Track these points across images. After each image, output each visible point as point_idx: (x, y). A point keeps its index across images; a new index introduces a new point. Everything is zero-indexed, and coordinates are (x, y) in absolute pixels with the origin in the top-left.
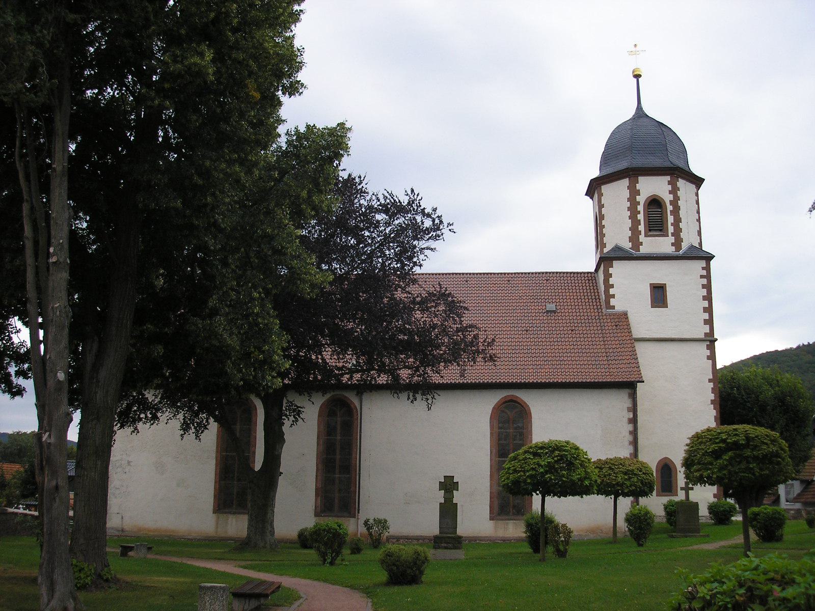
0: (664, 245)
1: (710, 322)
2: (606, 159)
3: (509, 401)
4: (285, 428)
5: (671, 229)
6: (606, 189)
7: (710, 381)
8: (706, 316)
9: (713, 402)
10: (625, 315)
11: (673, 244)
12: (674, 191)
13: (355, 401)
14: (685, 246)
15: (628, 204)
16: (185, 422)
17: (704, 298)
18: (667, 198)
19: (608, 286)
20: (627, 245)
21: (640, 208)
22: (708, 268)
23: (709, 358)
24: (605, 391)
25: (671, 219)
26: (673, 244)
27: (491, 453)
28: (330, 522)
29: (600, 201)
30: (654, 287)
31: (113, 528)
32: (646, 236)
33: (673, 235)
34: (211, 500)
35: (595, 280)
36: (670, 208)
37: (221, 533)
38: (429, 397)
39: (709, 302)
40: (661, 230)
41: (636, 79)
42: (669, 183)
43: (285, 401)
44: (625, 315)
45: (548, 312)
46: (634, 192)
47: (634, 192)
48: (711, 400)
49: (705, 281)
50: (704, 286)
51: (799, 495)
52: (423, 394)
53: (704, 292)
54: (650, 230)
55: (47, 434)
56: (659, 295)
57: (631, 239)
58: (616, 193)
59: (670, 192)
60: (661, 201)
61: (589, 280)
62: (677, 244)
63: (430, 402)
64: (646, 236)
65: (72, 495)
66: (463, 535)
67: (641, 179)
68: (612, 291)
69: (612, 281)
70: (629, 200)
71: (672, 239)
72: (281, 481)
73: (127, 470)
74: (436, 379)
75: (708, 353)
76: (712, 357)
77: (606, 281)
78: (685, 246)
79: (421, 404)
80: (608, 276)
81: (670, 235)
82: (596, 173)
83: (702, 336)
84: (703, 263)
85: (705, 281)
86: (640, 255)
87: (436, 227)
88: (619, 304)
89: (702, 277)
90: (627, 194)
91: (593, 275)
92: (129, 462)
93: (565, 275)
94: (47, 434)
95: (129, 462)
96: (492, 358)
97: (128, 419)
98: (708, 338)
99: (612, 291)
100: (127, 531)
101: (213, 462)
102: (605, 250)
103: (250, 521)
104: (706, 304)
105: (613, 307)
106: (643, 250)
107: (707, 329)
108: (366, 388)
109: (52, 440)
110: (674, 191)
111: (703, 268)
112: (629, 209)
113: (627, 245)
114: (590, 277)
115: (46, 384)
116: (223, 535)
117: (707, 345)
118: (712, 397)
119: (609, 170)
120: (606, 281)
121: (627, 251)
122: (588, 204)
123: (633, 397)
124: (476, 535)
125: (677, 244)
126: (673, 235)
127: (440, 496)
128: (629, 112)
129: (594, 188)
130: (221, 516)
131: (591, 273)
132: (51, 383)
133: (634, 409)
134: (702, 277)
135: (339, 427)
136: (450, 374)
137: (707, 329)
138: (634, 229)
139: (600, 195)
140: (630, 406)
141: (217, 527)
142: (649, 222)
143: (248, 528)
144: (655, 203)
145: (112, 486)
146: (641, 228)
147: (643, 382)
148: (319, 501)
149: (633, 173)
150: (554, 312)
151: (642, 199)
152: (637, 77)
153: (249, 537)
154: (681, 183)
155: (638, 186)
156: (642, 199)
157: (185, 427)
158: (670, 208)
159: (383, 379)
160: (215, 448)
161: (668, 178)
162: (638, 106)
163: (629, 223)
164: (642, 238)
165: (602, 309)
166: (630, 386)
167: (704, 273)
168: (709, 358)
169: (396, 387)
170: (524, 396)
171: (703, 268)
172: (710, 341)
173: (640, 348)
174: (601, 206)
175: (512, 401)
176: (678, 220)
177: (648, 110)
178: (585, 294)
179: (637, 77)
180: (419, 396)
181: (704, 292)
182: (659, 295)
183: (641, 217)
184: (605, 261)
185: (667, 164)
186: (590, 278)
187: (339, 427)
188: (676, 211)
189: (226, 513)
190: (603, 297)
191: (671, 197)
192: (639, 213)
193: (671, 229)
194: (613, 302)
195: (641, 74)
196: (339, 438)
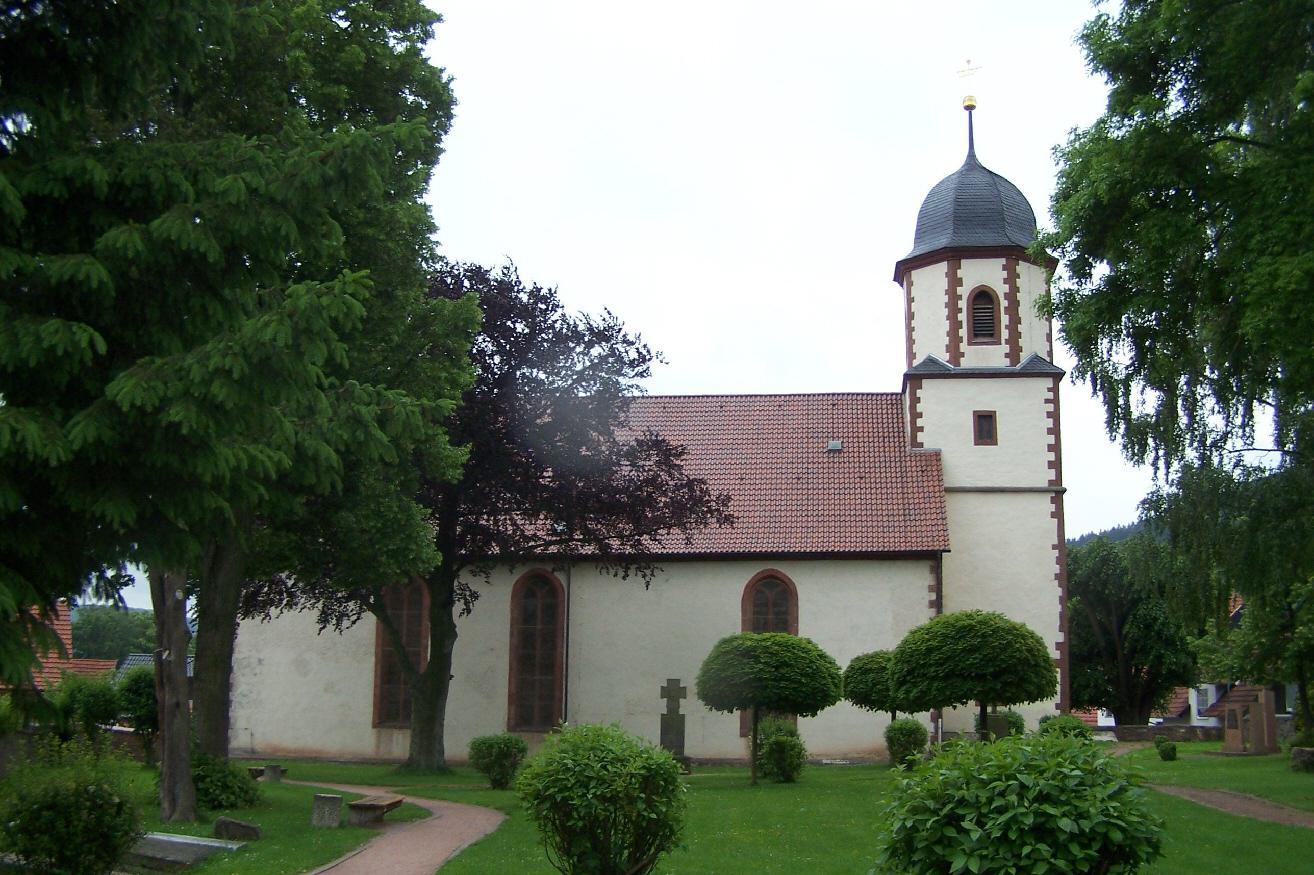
0: (995, 356)
1: (1056, 465)
2: (921, 233)
3: (765, 578)
4: (1158, 393)
5: (1005, 334)
6: (917, 275)
7: (1054, 547)
8: (1052, 456)
9: (1057, 577)
10: (937, 455)
11: (1007, 355)
12: (1012, 279)
13: (561, 577)
14: (1024, 357)
15: (946, 299)
16: (323, 612)
17: (1050, 431)
18: (1001, 289)
19: (916, 415)
20: (943, 357)
21: (963, 304)
22: (1055, 390)
23: (1053, 515)
24: (899, 563)
25: (1005, 319)
26: (1007, 355)
27: (511, 669)
28: (514, 736)
29: (909, 293)
30: (979, 416)
31: (238, 749)
32: (970, 344)
33: (1007, 342)
34: (370, 709)
35: (901, 404)
36: (1004, 303)
37: (384, 754)
38: (648, 572)
39: (1056, 437)
40: (991, 335)
41: (967, 112)
42: (1005, 268)
43: (456, 583)
44: (937, 455)
45: (830, 451)
46: (955, 282)
47: (955, 282)
48: (1056, 575)
49: (1051, 407)
50: (1049, 415)
51: (1212, 706)
52: (639, 569)
53: (1050, 423)
54: (976, 336)
55: (167, 652)
56: (985, 427)
57: (948, 349)
58: (932, 280)
59: (1006, 281)
60: (992, 293)
61: (892, 404)
62: (1014, 353)
63: (647, 579)
64: (970, 344)
65: (191, 702)
66: (692, 756)
67: (964, 262)
68: (920, 422)
69: (920, 408)
70: (947, 292)
71: (1005, 348)
72: (453, 687)
73: (257, 671)
74: (655, 548)
75: (1053, 508)
76: (1059, 514)
77: (913, 407)
78: (1024, 357)
79: (635, 582)
80: (915, 400)
81: (1003, 341)
82: (906, 248)
83: (1045, 484)
84: (1049, 383)
85: (1051, 407)
86: (960, 372)
87: (643, 359)
88: (928, 440)
89: (1047, 401)
90: (944, 283)
91: (899, 397)
92: (260, 661)
93: (859, 398)
94: (167, 652)
95: (260, 661)
96: (728, 520)
97: (255, 605)
98: (1054, 488)
99: (920, 422)
100: (258, 753)
101: (373, 659)
102: (916, 363)
103: (413, 736)
104: (1051, 439)
105: (921, 445)
106: (966, 363)
107: (1052, 474)
108: (571, 561)
109: (172, 658)
110: (1012, 279)
111: (1049, 390)
112: (947, 305)
113: (943, 357)
114: (895, 399)
115: (164, 604)
116: (386, 756)
117: (1052, 498)
118: (1057, 569)
119: (924, 249)
120: (913, 407)
121: (943, 366)
122: (898, 292)
123: (937, 571)
124: (722, 757)
125: (1014, 353)
126: (1007, 342)
127: (662, 706)
128: (956, 162)
129: (904, 270)
130: (385, 732)
131: (897, 394)
132: (169, 603)
133: (938, 588)
134: (1047, 401)
135: (539, 613)
136: (672, 541)
137: (1052, 474)
138: (953, 333)
139: (910, 284)
140: (933, 583)
141: (378, 747)
142: (974, 327)
143: (411, 747)
144: (983, 297)
145: (239, 692)
146: (963, 332)
147: (949, 551)
148: (512, 712)
149: (953, 255)
150: (839, 451)
151: (964, 291)
152: (970, 108)
153: (411, 758)
154: (1022, 268)
155: (960, 273)
156: (964, 291)
157: (324, 620)
158: (1004, 303)
159: (589, 550)
160: (373, 641)
161: (1003, 261)
162: (969, 152)
163: (946, 325)
164: (964, 347)
165: (905, 447)
166: (932, 558)
167: (1051, 395)
168: (1053, 515)
169: (606, 560)
170: (785, 569)
171: (1049, 390)
172: (1056, 491)
173: (954, 503)
174: (910, 300)
175: (772, 577)
176: (1015, 320)
177: (985, 159)
178: (895, 421)
179: (970, 108)
180: (631, 572)
181: (1050, 423)
182: (985, 427)
183: (963, 317)
184: (913, 379)
185: (1004, 241)
186: (894, 402)
187: (539, 613)
188: (1014, 305)
189: (390, 727)
190: (908, 428)
191: (1006, 289)
192: (960, 310)
193: (1005, 334)
194: (921, 437)
195: (974, 103)
196: (539, 627)
